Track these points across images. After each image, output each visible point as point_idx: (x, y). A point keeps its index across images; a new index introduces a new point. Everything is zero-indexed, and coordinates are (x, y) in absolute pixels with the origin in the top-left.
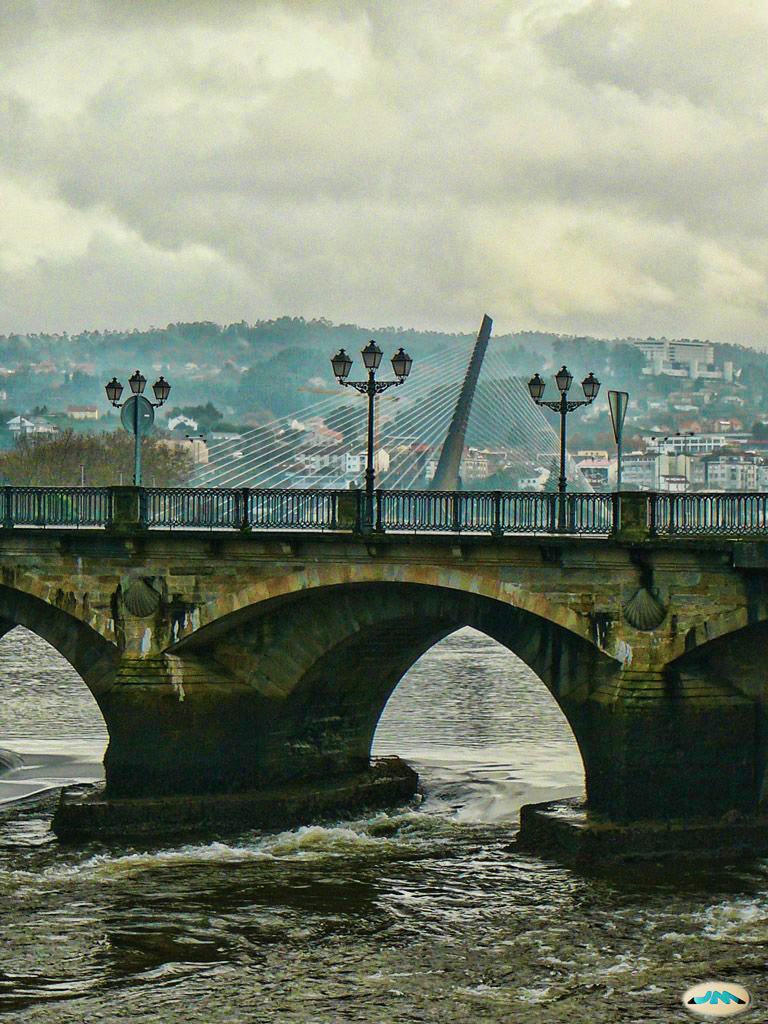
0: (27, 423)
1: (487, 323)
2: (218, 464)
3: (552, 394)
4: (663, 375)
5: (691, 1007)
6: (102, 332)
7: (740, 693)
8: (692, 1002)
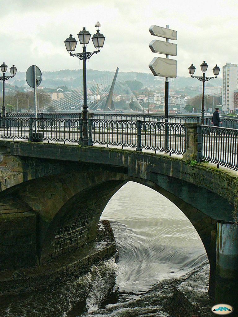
0: (28, 90)
1: (118, 69)
2: (66, 98)
3: (199, 73)
4: (158, 80)
5: (214, 312)
6: (47, 72)
7: (31, 210)
8: (214, 310)
